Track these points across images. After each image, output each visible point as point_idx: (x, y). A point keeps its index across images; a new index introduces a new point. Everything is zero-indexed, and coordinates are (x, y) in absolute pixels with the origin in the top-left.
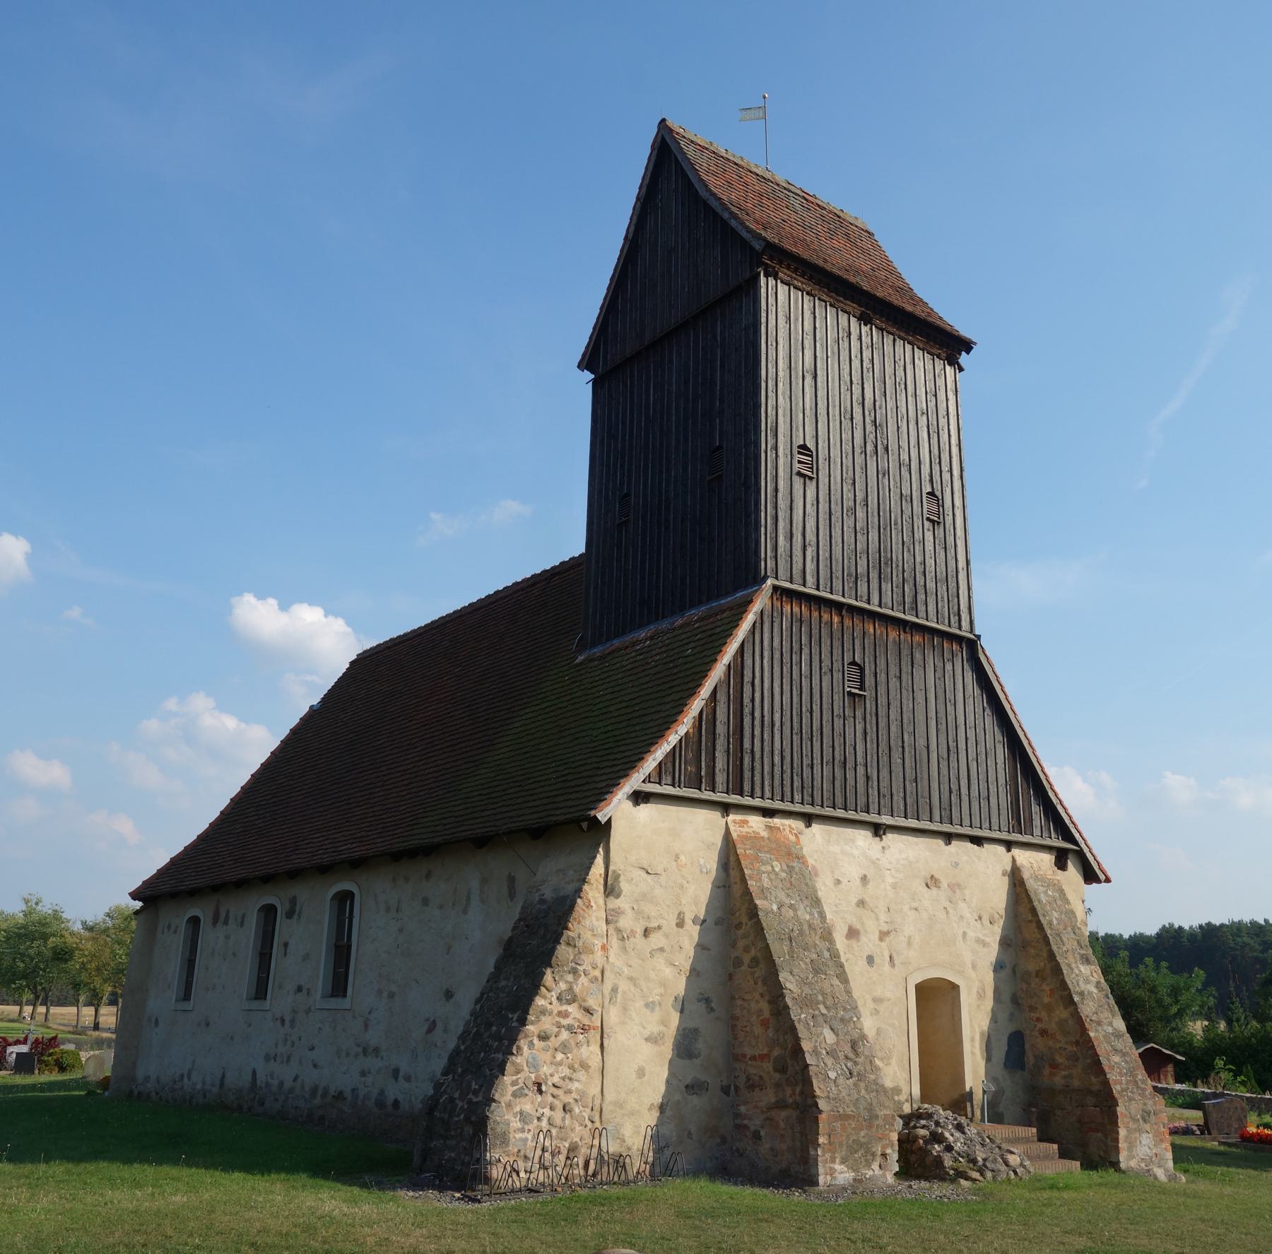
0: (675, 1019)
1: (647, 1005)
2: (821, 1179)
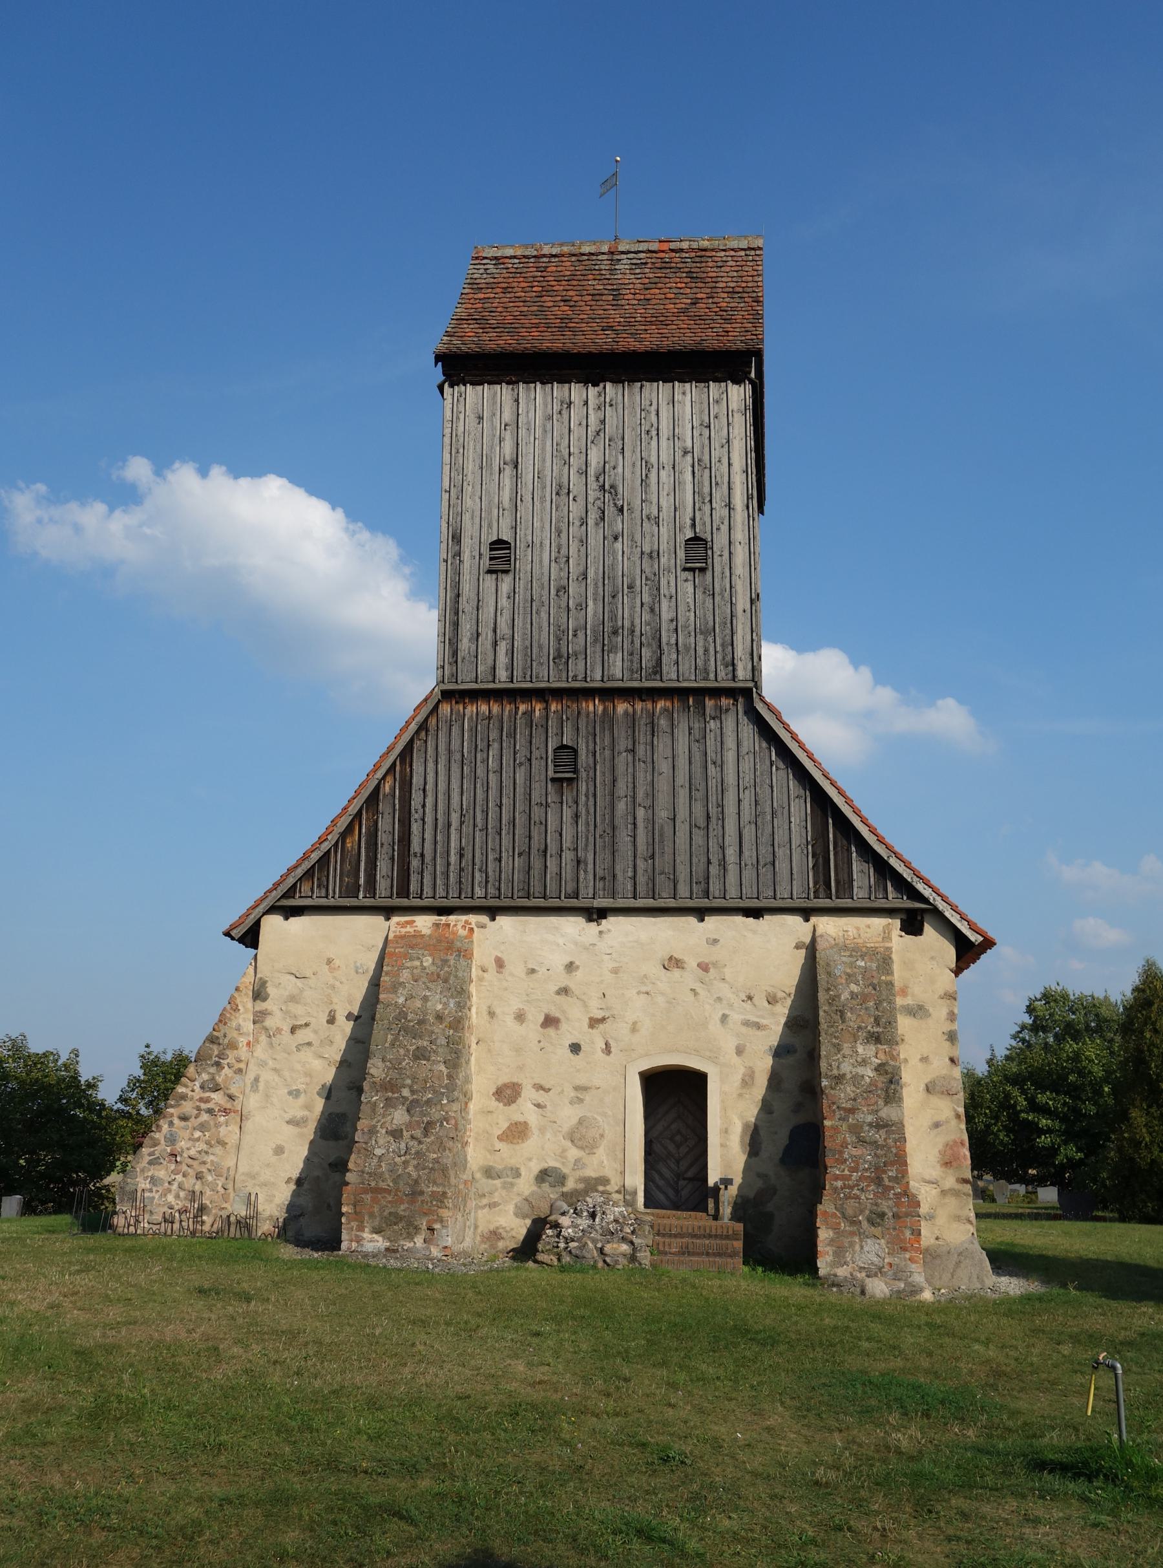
0: (319, 1104)
1: (290, 1093)
2: (344, 1246)
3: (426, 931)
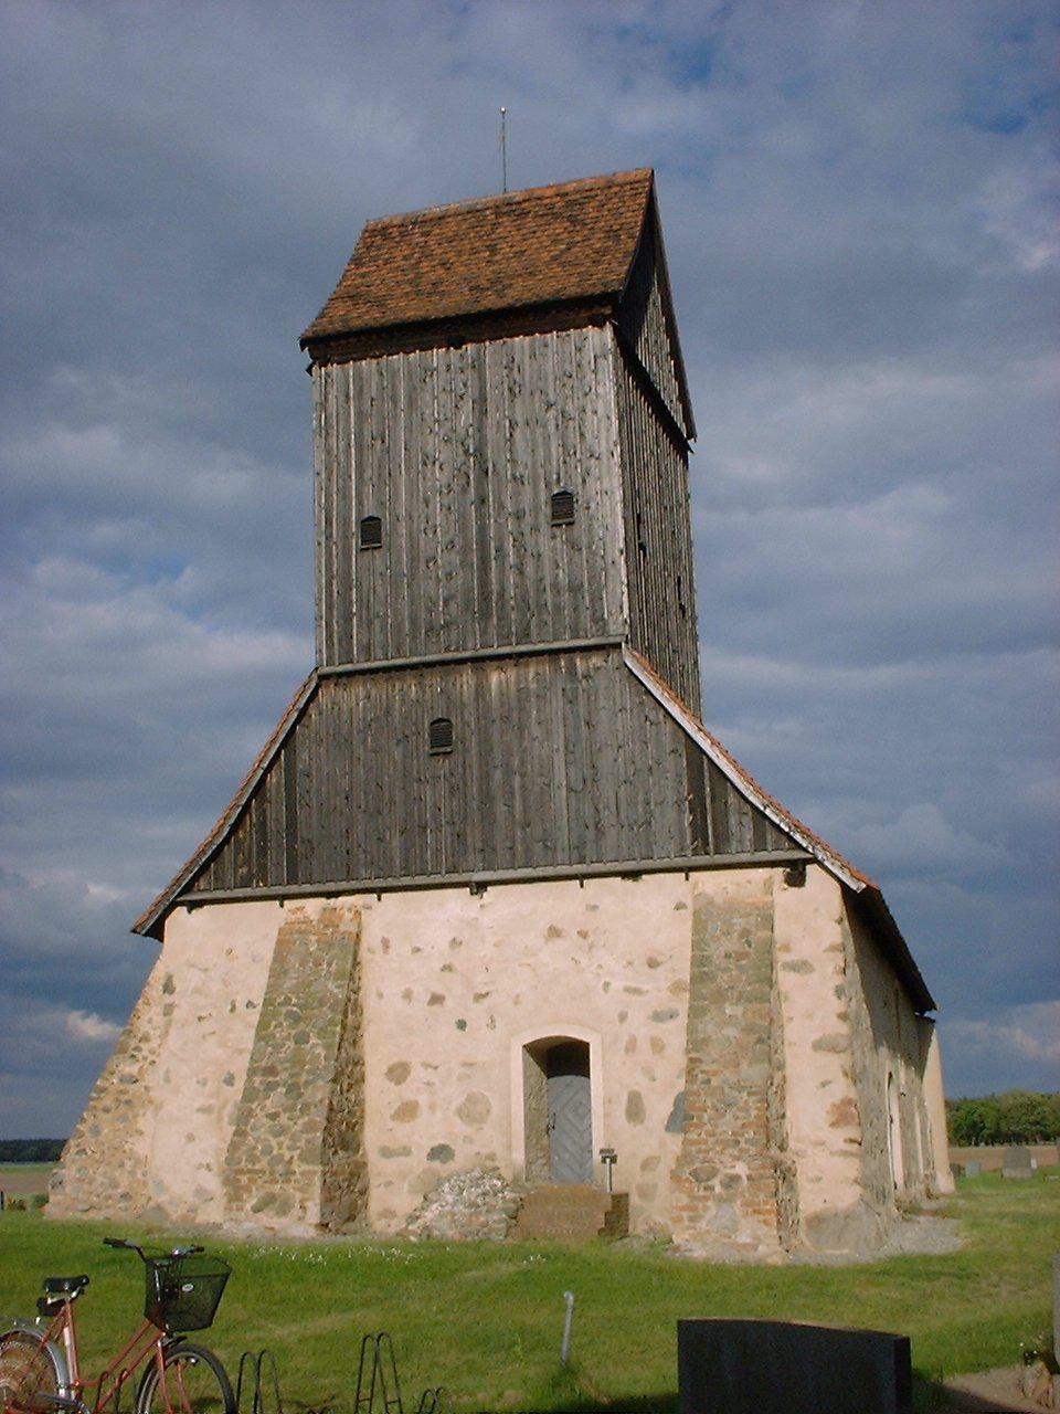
3: (314, 917)
